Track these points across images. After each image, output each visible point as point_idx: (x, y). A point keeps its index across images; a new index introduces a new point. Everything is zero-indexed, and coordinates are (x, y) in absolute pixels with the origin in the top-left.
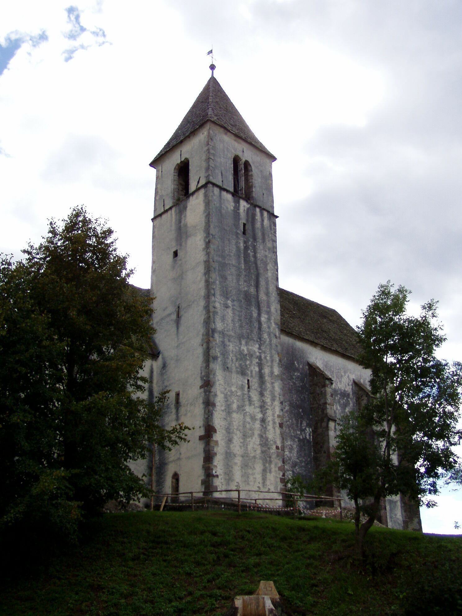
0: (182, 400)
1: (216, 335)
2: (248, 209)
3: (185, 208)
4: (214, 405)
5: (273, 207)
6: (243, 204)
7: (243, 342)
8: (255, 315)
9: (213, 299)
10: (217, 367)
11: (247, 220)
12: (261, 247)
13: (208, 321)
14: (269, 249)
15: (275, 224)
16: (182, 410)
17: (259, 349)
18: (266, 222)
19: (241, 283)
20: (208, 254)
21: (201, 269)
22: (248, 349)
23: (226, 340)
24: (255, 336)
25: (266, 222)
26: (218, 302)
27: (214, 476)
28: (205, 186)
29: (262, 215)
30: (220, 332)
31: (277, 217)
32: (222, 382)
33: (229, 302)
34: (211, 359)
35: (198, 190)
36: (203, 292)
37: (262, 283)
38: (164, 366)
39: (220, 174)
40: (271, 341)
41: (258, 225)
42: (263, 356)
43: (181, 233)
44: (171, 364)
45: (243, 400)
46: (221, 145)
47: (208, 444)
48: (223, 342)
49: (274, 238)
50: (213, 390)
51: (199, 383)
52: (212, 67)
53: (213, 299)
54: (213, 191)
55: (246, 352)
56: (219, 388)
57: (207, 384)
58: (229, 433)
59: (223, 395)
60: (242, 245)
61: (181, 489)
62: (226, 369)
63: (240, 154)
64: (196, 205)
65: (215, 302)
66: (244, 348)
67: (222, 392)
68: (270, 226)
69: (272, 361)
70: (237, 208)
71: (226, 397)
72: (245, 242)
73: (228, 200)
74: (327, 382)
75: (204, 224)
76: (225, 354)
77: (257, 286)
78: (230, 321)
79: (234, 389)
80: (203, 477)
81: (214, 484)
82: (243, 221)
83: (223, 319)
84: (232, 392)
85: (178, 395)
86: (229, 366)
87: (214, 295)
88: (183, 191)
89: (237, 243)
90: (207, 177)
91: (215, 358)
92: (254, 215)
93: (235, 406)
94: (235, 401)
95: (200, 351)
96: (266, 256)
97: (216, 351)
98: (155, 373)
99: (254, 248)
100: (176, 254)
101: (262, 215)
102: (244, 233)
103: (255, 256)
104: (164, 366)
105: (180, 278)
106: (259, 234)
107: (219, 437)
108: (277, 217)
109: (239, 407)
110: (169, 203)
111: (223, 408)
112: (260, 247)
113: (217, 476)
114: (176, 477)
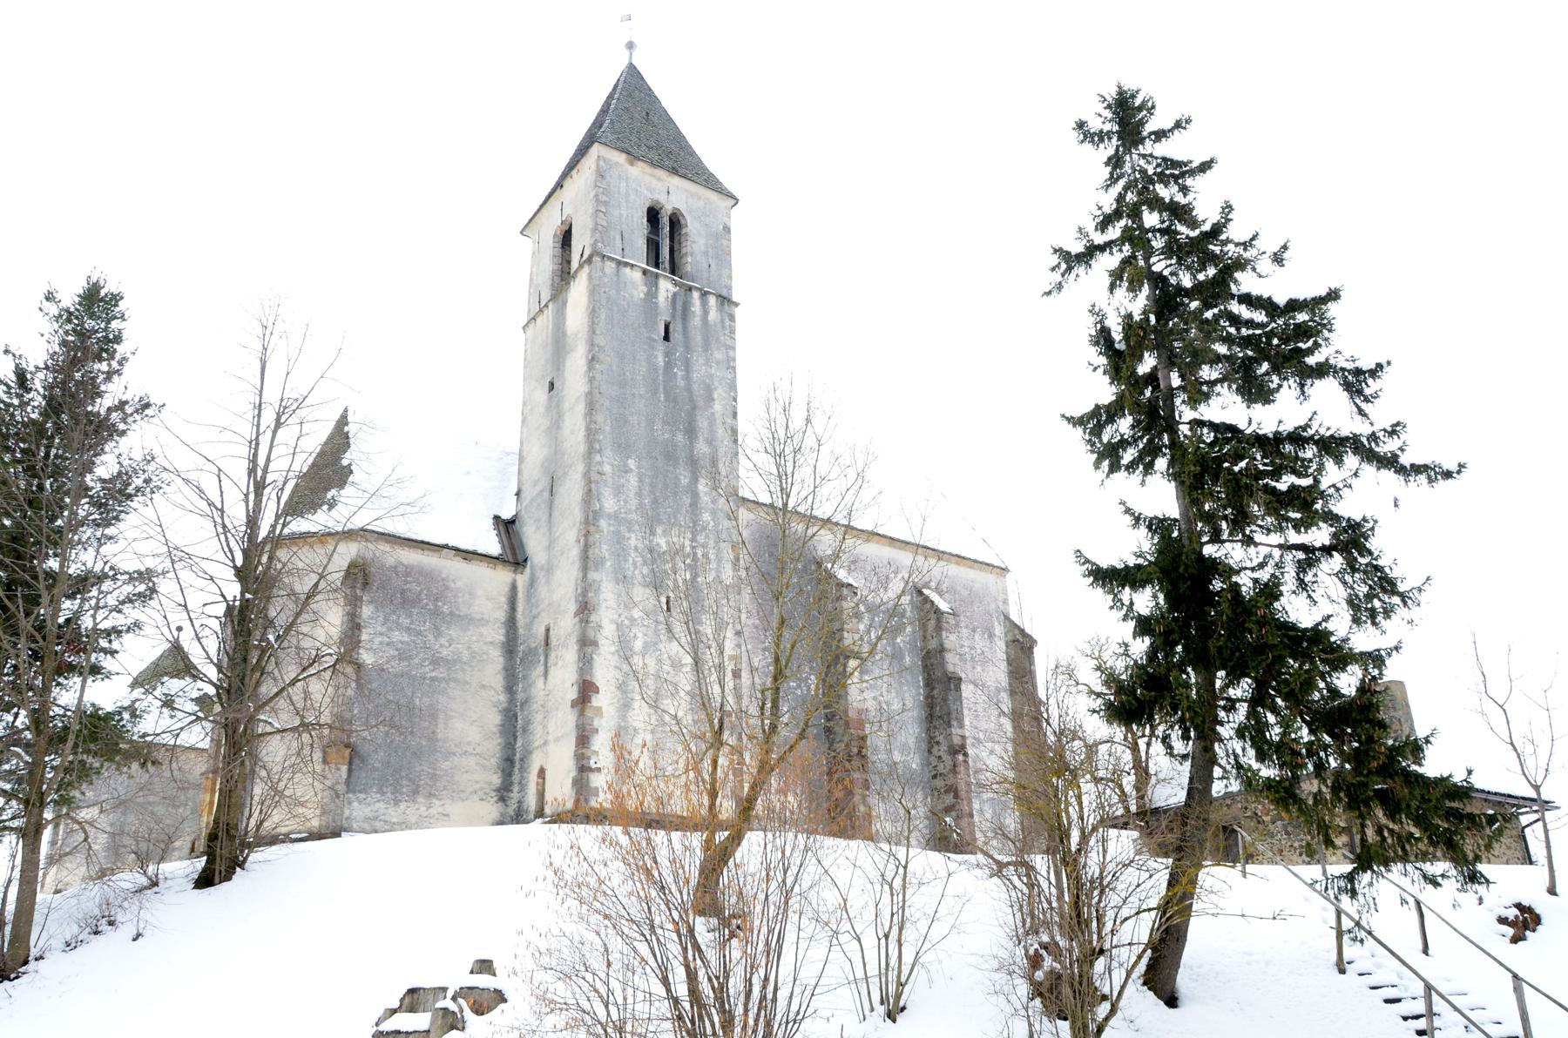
0: (554, 641)
1: (603, 523)
2: (675, 294)
3: (564, 304)
4: (595, 644)
5: (729, 288)
6: (666, 287)
7: (659, 531)
8: (685, 481)
9: (598, 458)
10: (605, 581)
11: (673, 316)
12: (701, 361)
13: (589, 496)
14: (718, 363)
15: (732, 318)
16: (553, 655)
17: (692, 540)
18: (713, 315)
19: (658, 426)
20: (591, 380)
21: (581, 408)
22: (668, 543)
23: (623, 529)
24: (684, 518)
25: (713, 315)
26: (607, 463)
27: (591, 770)
28: (589, 261)
29: (704, 304)
30: (609, 516)
31: (737, 305)
32: (612, 603)
33: (632, 463)
34: (591, 564)
35: (581, 266)
36: (582, 448)
37: (702, 423)
38: (532, 582)
39: (618, 237)
40: (717, 525)
41: (696, 321)
42: (700, 553)
43: (559, 345)
44: (541, 575)
45: (656, 631)
46: (623, 184)
47: (582, 713)
48: (617, 533)
49: (729, 342)
50: (593, 618)
51: (572, 607)
52: (630, 46)
53: (598, 458)
54: (602, 269)
55: (664, 547)
56: (606, 618)
57: (585, 609)
58: (625, 692)
59: (614, 627)
60: (660, 360)
61: (548, 797)
62: (623, 579)
63: (662, 199)
64: (578, 291)
65: (601, 464)
66: (661, 542)
67: (612, 621)
68: (722, 321)
69: (719, 560)
70: (652, 294)
71: (619, 626)
72: (667, 354)
73: (633, 283)
74: (845, 591)
75: (586, 328)
76: (620, 554)
77: (691, 432)
78: (632, 495)
79: (637, 614)
80: (573, 774)
81: (593, 785)
82: (665, 316)
83: (618, 491)
84: (632, 620)
85: (548, 630)
86: (629, 573)
87: (600, 451)
88: (564, 275)
89: (650, 360)
90: (594, 244)
91: (599, 564)
92: (686, 306)
93: (638, 645)
94: (640, 635)
95: (575, 552)
96: (711, 376)
97: (603, 549)
98: (520, 595)
99: (687, 365)
100: (552, 386)
101: (704, 304)
102: (666, 338)
103: (687, 378)
104: (532, 582)
105: (556, 425)
106: (697, 338)
107: (604, 700)
108: (737, 305)
109: (646, 646)
110: (546, 297)
111: (613, 649)
112: (698, 361)
113: (599, 770)
114: (542, 773)
